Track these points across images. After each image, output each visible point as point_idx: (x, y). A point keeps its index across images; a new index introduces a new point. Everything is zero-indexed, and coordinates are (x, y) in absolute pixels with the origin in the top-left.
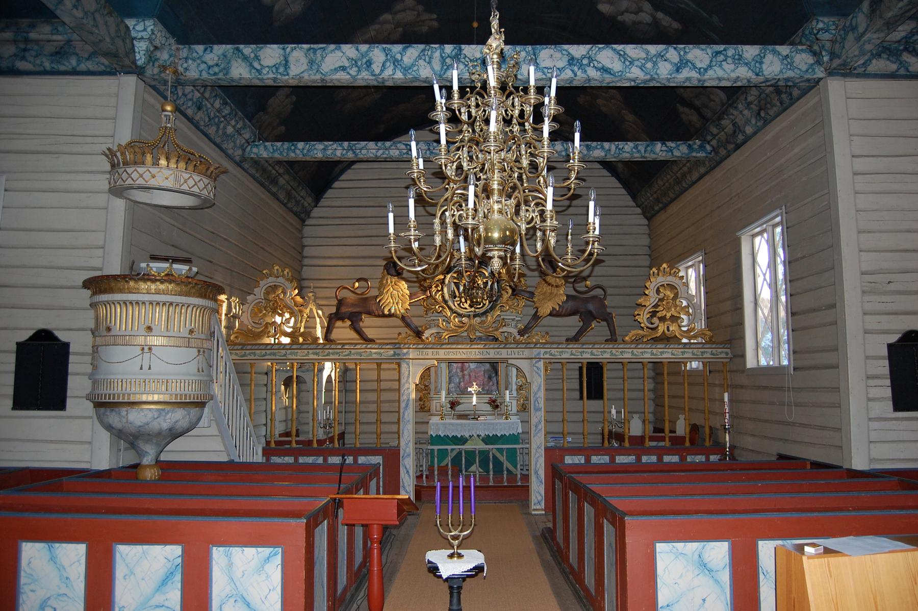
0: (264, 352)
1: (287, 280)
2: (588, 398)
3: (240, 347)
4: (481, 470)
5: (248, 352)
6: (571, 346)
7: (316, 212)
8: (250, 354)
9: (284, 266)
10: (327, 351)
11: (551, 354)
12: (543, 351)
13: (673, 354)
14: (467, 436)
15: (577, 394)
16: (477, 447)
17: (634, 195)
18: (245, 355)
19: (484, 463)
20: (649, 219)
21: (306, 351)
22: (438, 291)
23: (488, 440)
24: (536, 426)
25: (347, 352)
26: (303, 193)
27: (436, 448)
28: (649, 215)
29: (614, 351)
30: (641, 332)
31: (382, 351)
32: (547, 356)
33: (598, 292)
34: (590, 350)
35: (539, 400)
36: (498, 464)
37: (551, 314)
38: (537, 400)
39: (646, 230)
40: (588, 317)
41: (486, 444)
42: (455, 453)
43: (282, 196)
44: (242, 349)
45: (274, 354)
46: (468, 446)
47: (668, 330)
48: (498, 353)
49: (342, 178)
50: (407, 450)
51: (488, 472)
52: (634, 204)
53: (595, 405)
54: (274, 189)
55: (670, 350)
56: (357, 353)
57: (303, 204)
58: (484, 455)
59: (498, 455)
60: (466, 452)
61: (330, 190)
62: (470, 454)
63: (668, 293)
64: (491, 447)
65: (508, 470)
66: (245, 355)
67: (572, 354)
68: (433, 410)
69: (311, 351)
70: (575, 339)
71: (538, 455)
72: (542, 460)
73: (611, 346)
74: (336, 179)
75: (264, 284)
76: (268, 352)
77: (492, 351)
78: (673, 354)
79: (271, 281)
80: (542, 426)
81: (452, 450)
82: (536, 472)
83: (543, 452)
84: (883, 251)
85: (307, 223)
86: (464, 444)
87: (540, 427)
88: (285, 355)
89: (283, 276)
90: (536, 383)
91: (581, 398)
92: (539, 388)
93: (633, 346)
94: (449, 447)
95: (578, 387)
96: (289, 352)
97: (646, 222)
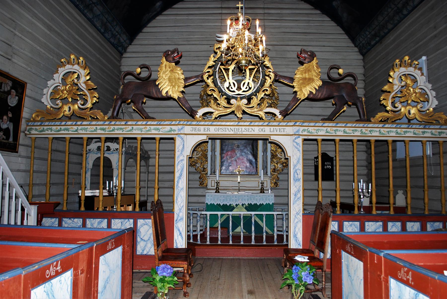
0: (59, 127)
1: (81, 67)
2: (323, 180)
3: (39, 124)
4: (244, 231)
5: (45, 128)
6: (326, 125)
7: (131, 48)
8: (47, 130)
9: (79, 54)
10: (112, 127)
11: (309, 132)
12: (302, 128)
13: (414, 134)
14: (234, 205)
15: (313, 177)
16: (242, 213)
17: (353, 39)
18: (43, 130)
19: (247, 226)
20: (363, 54)
21: (95, 127)
22: (210, 76)
23: (250, 207)
24: (295, 195)
25: (130, 127)
26: (118, 29)
27: (208, 213)
28: (364, 51)
29: (364, 130)
30: (386, 114)
31: (160, 127)
32: (305, 133)
33: (349, 80)
34: (343, 129)
35: (298, 172)
36: (259, 228)
37: (308, 99)
38: (296, 171)
39: (361, 63)
40: (341, 102)
41: (248, 211)
42: (224, 217)
43: (98, 24)
44: (41, 125)
45: (67, 130)
46: (235, 212)
47: (410, 113)
48: (262, 130)
49: (150, 25)
50: (181, 214)
51: (251, 232)
52: (353, 45)
53: (328, 184)
54: (90, 16)
55: (412, 130)
56: (138, 129)
57: (119, 40)
58: (248, 219)
59: (257, 220)
60: (232, 216)
61: (145, 28)
62: (236, 219)
63: (409, 82)
64: (253, 213)
65: (266, 232)
66: (43, 130)
67: (327, 132)
68: (209, 187)
69: (99, 127)
70: (330, 118)
71: (296, 220)
72: (300, 226)
73: (361, 125)
74: (145, 25)
75: (62, 71)
76: (63, 128)
77: (256, 128)
78: (414, 134)
79: (68, 68)
80: (300, 195)
81: (222, 215)
82: (295, 236)
83: (301, 218)
84: (348, 166)
85: (124, 56)
86: (231, 211)
87: (299, 196)
88: (76, 131)
89: (78, 64)
90: (295, 157)
91: (317, 179)
92: (298, 162)
93: (381, 125)
94: (219, 213)
95: (313, 171)
96: (80, 127)
97: (361, 57)
